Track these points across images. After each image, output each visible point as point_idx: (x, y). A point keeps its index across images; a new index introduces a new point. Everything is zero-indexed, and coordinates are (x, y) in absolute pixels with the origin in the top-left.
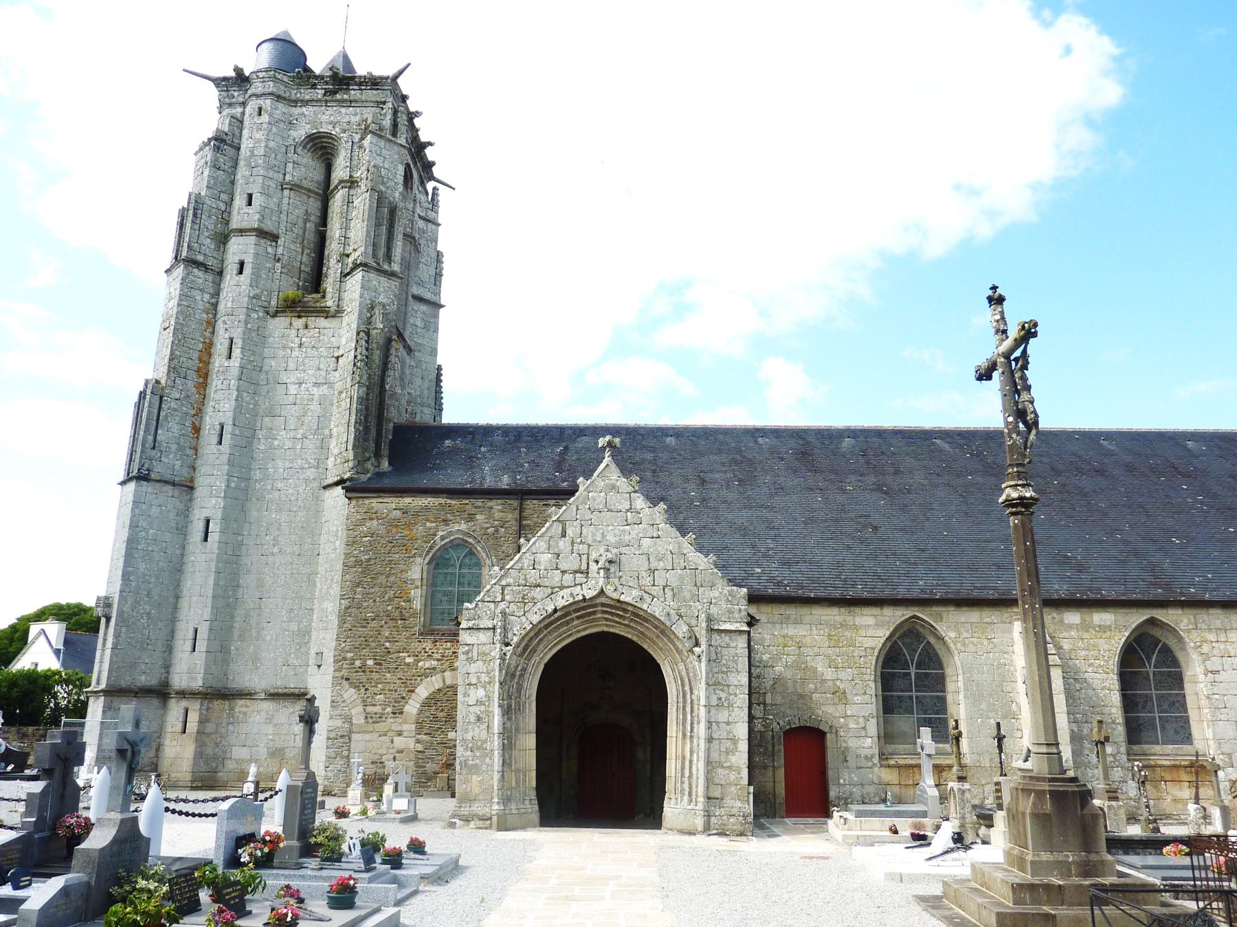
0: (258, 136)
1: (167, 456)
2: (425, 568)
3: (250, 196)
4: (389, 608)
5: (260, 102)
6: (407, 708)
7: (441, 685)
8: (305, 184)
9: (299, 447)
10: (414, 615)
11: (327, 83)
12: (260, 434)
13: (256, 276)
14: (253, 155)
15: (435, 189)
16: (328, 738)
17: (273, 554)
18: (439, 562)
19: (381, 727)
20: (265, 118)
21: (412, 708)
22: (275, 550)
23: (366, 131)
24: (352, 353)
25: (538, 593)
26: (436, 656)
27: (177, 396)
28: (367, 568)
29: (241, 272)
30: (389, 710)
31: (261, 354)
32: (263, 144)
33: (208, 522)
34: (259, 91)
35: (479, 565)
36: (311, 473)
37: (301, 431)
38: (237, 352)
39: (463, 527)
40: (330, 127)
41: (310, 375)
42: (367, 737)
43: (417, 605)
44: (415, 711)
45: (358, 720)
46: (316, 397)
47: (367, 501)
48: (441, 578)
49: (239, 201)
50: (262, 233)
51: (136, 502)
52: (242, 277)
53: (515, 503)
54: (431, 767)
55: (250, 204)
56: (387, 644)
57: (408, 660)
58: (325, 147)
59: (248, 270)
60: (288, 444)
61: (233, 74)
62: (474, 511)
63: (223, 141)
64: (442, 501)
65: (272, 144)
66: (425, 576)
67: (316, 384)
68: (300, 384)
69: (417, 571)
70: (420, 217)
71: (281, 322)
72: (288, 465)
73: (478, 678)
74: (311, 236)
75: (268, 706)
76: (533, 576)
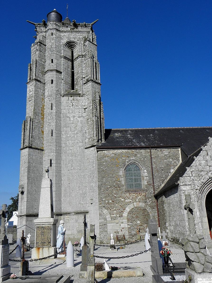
0: (52, 42)
1: (36, 140)
2: (124, 171)
3: (52, 60)
4: (114, 184)
5: (52, 31)
6: (124, 215)
7: (133, 207)
8: (67, 56)
9: (76, 136)
10: (123, 186)
11: (71, 26)
12: (63, 133)
13: (57, 84)
14: (51, 47)
16: (100, 226)
17: (71, 170)
18: (127, 169)
19: (116, 221)
20: (54, 36)
21: (125, 214)
23: (85, 40)
24: (91, 107)
25: (202, 173)
26: (131, 198)
27: (37, 122)
28: (103, 172)
29: (52, 83)
30: (118, 215)
31: (61, 108)
32: (54, 44)
33: (51, 160)
34: (51, 28)
35: (139, 170)
36: (81, 144)
38: (54, 108)
39: (134, 158)
40: (74, 39)
41: (77, 114)
42: (112, 224)
43: (123, 183)
44: (126, 215)
45: (109, 219)
46: (80, 121)
47: (103, 152)
48: (128, 175)
49: (48, 62)
50: (58, 71)
51: (29, 155)
52: (53, 85)
53: (149, 150)
54: (133, 232)
55: (52, 62)
56: (115, 195)
57: (122, 200)
58: (72, 46)
59: (54, 82)
60: (72, 135)
62: (136, 153)
63: (41, 43)
64: (126, 151)
65: (57, 44)
66: (124, 174)
67: (79, 117)
69: (121, 172)
71: (66, 98)
72: (73, 142)
74: (70, 73)
75: (75, 217)
76: (200, 168)
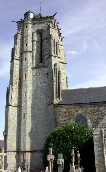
15: (62, 38)
17: (38, 121)
22: (39, 120)
37: (42, 93)
47: (59, 107)
61: (20, 20)
64: (75, 106)
67: (44, 83)
68: (40, 83)
70: (60, 45)
73: (99, 145)
